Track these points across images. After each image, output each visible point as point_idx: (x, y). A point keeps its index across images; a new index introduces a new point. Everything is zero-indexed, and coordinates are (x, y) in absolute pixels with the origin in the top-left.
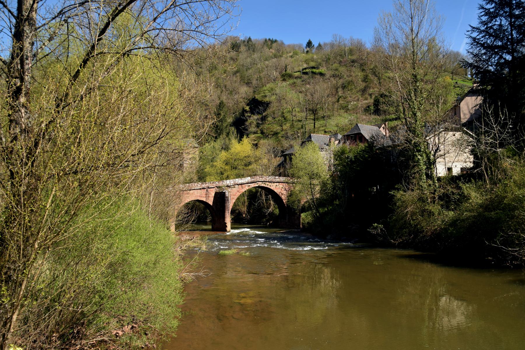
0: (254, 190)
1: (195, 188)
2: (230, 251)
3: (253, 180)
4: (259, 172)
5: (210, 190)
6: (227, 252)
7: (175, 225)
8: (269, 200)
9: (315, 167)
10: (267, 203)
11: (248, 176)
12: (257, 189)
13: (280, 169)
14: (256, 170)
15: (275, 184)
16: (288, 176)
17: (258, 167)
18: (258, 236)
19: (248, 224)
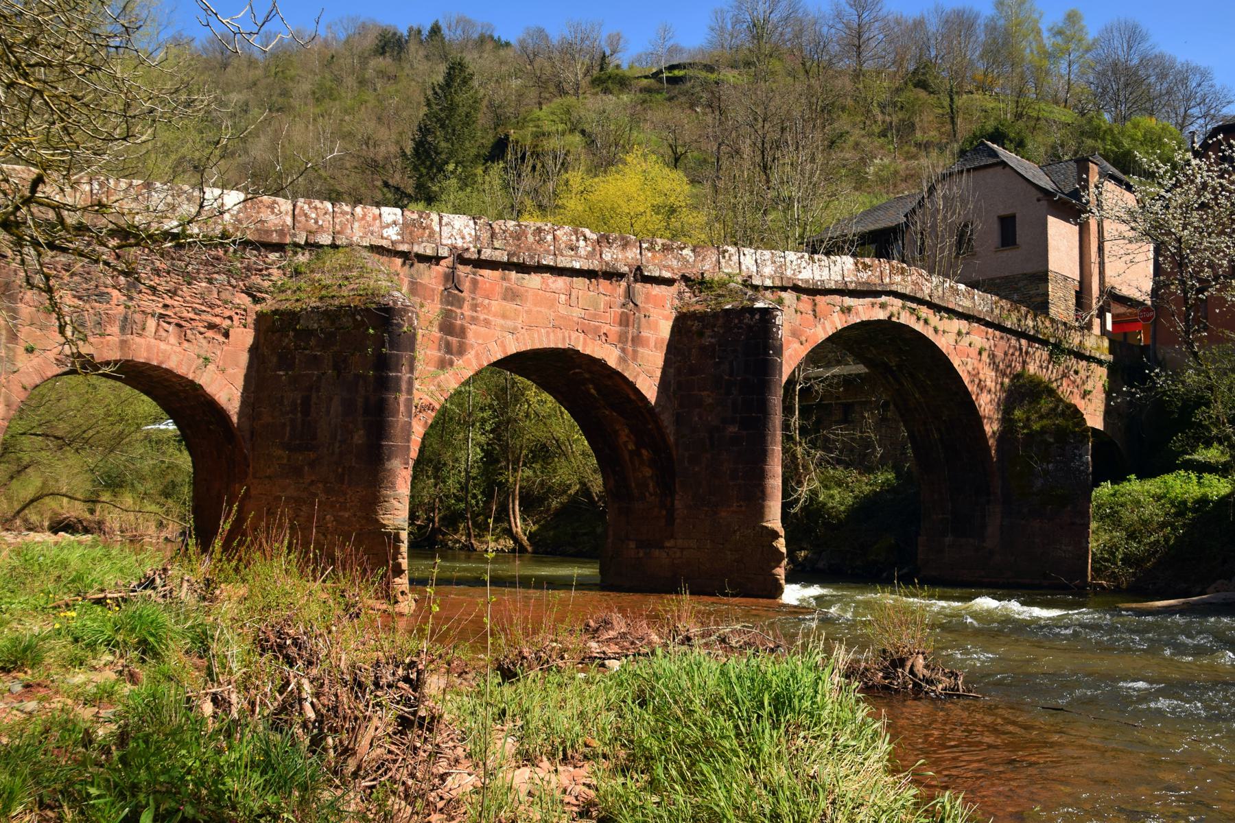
1: (563, 262)
3: (864, 276)
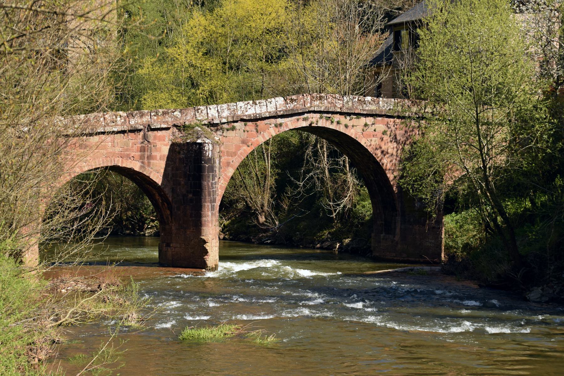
0: (295, 140)
1: (108, 129)
2: (214, 329)
3: (291, 106)
4: (312, 83)
5: (155, 138)
6: (204, 333)
7: (41, 244)
8: (342, 171)
9: (496, 65)
10: (334, 181)
11: (275, 95)
12: (305, 134)
13: (378, 74)
14: (302, 73)
15: (363, 120)
16: (406, 96)
17: (308, 65)
18: (303, 283)
19: (273, 245)
